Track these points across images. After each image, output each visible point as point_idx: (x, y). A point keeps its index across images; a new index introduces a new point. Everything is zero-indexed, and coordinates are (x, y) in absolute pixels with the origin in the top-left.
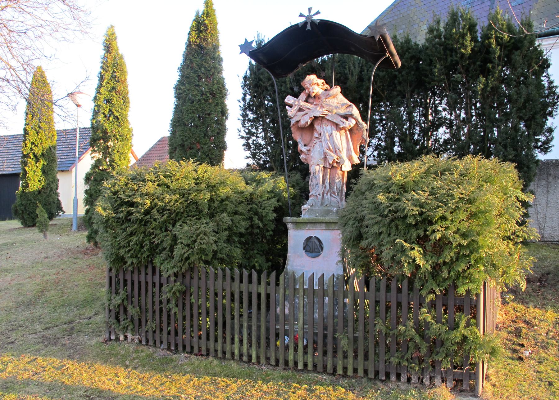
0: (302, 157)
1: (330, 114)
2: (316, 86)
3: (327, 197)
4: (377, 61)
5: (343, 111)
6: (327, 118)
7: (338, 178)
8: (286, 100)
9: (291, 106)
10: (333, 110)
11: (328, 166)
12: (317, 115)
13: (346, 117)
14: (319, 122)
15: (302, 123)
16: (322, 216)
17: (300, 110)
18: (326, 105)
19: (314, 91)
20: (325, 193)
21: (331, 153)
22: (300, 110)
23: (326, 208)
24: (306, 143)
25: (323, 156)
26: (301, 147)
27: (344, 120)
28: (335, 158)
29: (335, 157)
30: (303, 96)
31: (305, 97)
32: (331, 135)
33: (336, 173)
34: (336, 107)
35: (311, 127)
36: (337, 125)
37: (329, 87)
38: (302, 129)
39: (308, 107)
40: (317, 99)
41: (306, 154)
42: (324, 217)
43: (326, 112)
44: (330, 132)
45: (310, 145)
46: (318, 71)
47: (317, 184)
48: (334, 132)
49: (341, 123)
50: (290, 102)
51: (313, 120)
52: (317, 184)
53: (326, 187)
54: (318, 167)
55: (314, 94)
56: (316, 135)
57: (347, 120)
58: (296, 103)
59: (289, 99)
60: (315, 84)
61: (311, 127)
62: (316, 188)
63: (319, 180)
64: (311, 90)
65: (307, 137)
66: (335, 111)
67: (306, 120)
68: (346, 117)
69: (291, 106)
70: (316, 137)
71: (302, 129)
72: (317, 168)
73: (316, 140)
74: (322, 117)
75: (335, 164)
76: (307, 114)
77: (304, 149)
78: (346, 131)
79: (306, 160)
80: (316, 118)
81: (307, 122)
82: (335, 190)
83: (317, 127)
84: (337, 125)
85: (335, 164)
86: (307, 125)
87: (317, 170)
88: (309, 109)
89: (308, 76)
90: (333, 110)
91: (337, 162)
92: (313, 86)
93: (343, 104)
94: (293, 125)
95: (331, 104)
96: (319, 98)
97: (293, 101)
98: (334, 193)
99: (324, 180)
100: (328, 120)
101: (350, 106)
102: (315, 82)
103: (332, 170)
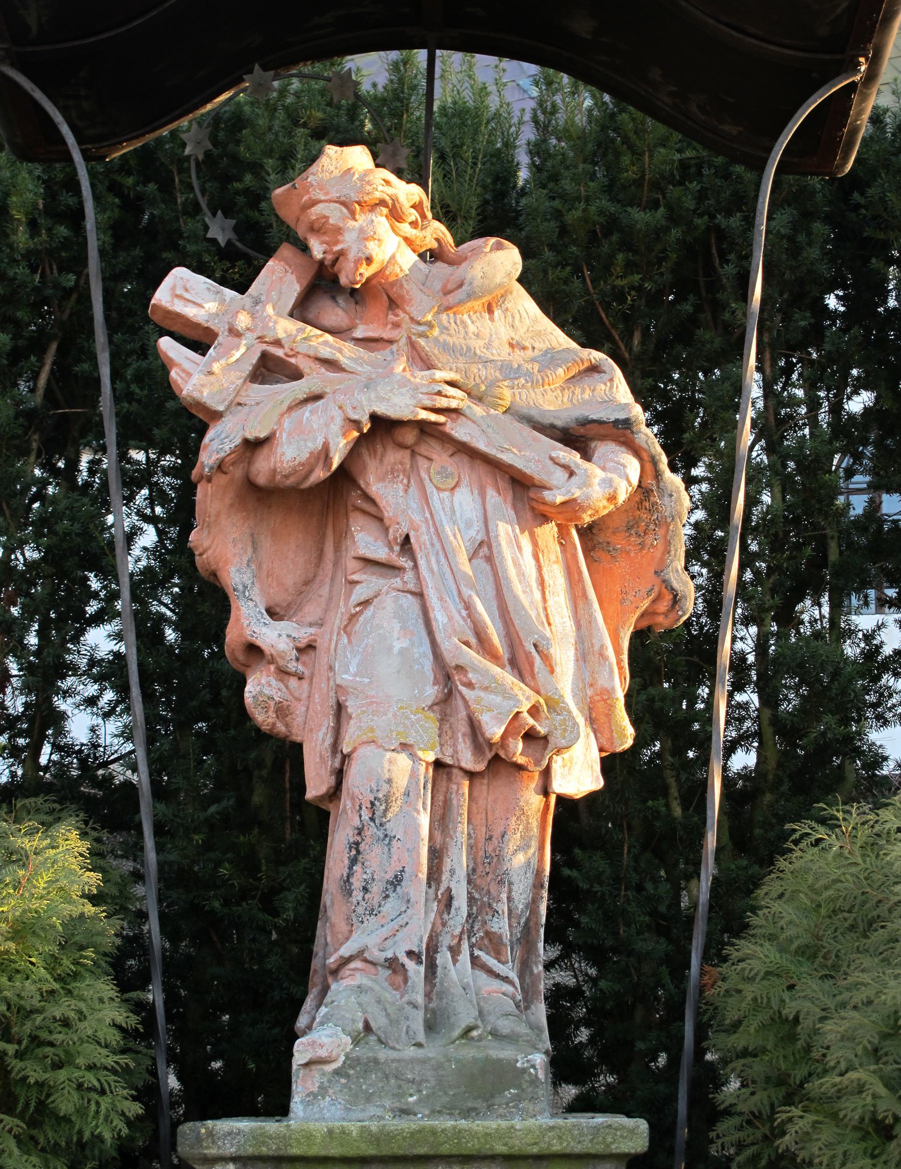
0: (259, 688)
1: (478, 411)
2: (381, 222)
3: (457, 971)
4: (775, 136)
5: (556, 402)
6: (460, 431)
7: (525, 847)
8: (162, 296)
9: (199, 341)
10: (493, 384)
11: (468, 760)
12: (400, 405)
13: (578, 437)
14: (394, 456)
15: (289, 454)
16: (450, 1110)
17: (270, 368)
18: (447, 348)
19: (372, 247)
20: (446, 941)
21: (496, 670)
22: (270, 368)
23: (469, 1053)
24: (280, 598)
25: (431, 692)
26: (249, 621)
27: (573, 457)
28: (525, 707)
29: (525, 697)
30: (279, 279)
31: (293, 289)
32: (485, 550)
33: (514, 807)
34: (510, 372)
35: (330, 497)
36: (520, 486)
37: (449, 238)
38: (265, 498)
39: (325, 353)
40: (377, 308)
41: (283, 673)
42: (467, 1113)
43: (456, 399)
44: (476, 533)
45: (312, 611)
46: (405, 138)
47: (396, 882)
48: (505, 531)
49: (560, 475)
50: (190, 312)
51: (363, 440)
52: (396, 882)
53: (448, 901)
54: (403, 761)
55: (367, 271)
56: (366, 541)
57: (587, 456)
58: (243, 321)
59: (185, 293)
60: (367, 205)
61: (330, 497)
62: (390, 907)
63: (416, 850)
64: (348, 241)
65: (288, 554)
66: (507, 395)
67: (307, 437)
68: (578, 437)
69: (199, 341)
70: (367, 562)
71: (265, 498)
72: (400, 768)
73: (369, 583)
74: (425, 429)
75: (517, 749)
76: (317, 397)
77: (274, 637)
78: (563, 532)
79: (282, 711)
80: (382, 428)
81: (325, 454)
82: (501, 926)
83: (383, 483)
84: (520, 486)
85: (517, 749)
86: (320, 474)
87: (401, 782)
88: (331, 364)
89: (331, 150)
90: (493, 384)
91: (530, 736)
92: (362, 219)
93: (551, 358)
94: (220, 467)
95: (478, 345)
96: (393, 304)
97: (212, 306)
98: (494, 943)
99: (436, 855)
100: (465, 450)
101: (594, 369)
102: (380, 192)
103: (482, 786)
